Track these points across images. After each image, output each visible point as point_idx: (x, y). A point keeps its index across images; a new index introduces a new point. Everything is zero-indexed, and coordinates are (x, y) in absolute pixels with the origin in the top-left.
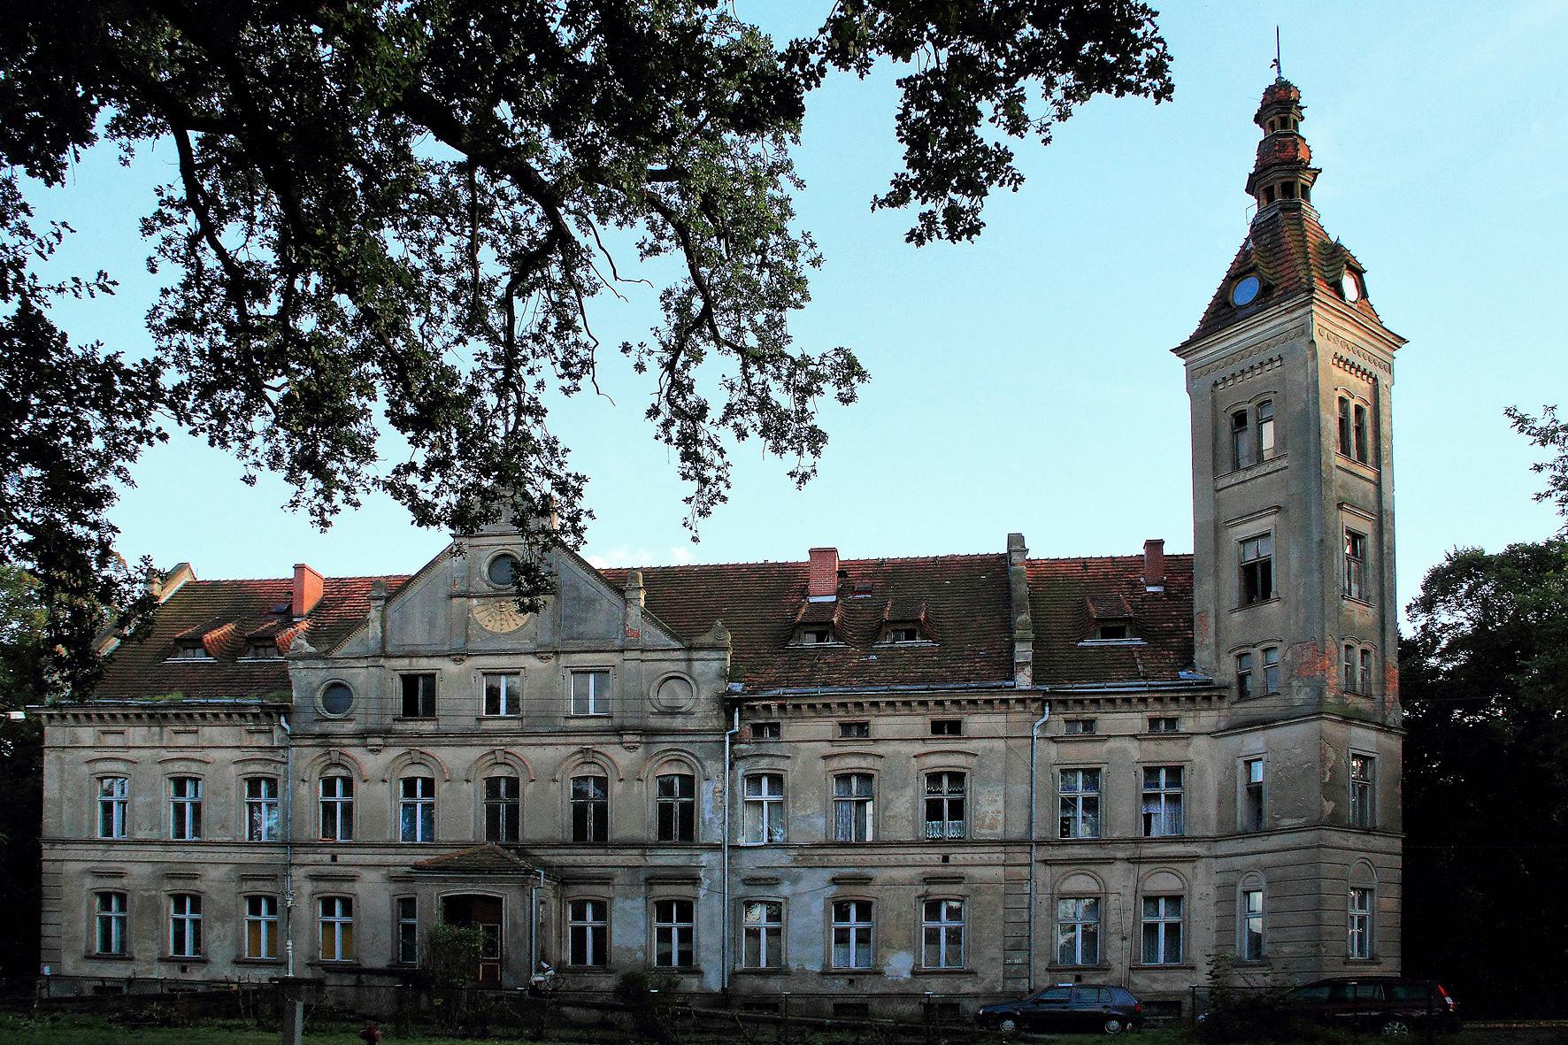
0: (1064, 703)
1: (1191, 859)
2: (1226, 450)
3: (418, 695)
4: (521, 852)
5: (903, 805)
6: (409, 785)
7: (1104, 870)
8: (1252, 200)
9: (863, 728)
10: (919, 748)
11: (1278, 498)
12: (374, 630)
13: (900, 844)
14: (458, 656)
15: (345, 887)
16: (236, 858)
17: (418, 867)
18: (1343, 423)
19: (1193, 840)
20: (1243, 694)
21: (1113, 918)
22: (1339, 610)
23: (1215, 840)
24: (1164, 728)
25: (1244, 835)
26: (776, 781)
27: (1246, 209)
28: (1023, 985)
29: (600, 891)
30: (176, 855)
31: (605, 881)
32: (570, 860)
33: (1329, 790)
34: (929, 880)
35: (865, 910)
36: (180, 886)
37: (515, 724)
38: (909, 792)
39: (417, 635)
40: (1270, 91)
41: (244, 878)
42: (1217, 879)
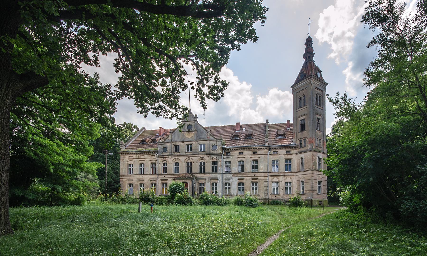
0: (273, 148)
1: (293, 176)
2: (298, 105)
3: (177, 149)
4: (192, 175)
5: (248, 167)
6: (176, 164)
7: (279, 177)
8: (304, 59)
9: (242, 153)
10: (251, 156)
11: (306, 112)
12: (170, 138)
13: (248, 173)
14: (183, 142)
15: (166, 181)
16: (150, 177)
17: (176, 178)
18: (317, 99)
19: (293, 172)
20: (301, 147)
21: (281, 186)
22: (316, 132)
23: (296, 172)
24: (288, 153)
25: (301, 171)
26: (230, 162)
27: (303, 60)
28: (267, 197)
29: (203, 181)
30: (141, 177)
31: (205, 180)
32: (199, 176)
33: (314, 164)
34: (252, 179)
35: (243, 184)
36: (141, 182)
37: (191, 153)
38: (249, 164)
39: (177, 138)
40: (307, 39)
41: (151, 180)
42: (297, 179)
